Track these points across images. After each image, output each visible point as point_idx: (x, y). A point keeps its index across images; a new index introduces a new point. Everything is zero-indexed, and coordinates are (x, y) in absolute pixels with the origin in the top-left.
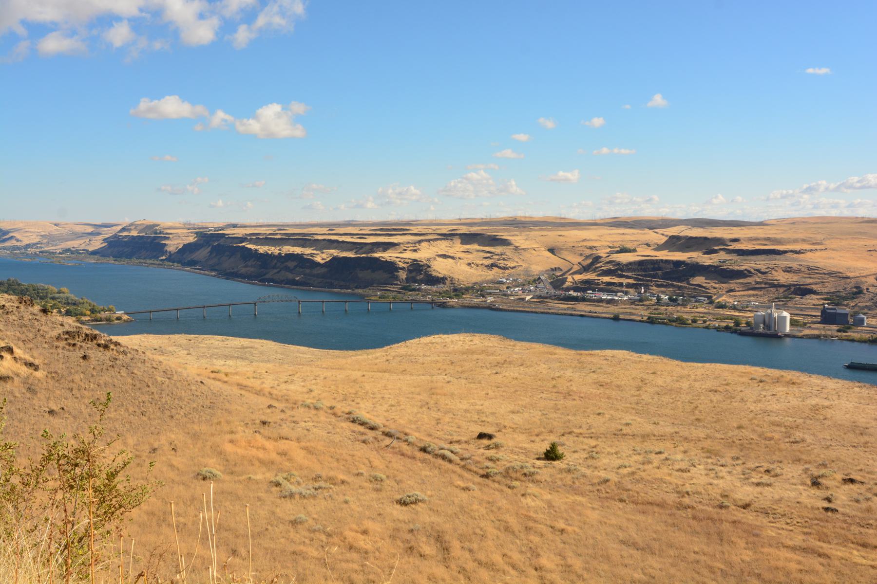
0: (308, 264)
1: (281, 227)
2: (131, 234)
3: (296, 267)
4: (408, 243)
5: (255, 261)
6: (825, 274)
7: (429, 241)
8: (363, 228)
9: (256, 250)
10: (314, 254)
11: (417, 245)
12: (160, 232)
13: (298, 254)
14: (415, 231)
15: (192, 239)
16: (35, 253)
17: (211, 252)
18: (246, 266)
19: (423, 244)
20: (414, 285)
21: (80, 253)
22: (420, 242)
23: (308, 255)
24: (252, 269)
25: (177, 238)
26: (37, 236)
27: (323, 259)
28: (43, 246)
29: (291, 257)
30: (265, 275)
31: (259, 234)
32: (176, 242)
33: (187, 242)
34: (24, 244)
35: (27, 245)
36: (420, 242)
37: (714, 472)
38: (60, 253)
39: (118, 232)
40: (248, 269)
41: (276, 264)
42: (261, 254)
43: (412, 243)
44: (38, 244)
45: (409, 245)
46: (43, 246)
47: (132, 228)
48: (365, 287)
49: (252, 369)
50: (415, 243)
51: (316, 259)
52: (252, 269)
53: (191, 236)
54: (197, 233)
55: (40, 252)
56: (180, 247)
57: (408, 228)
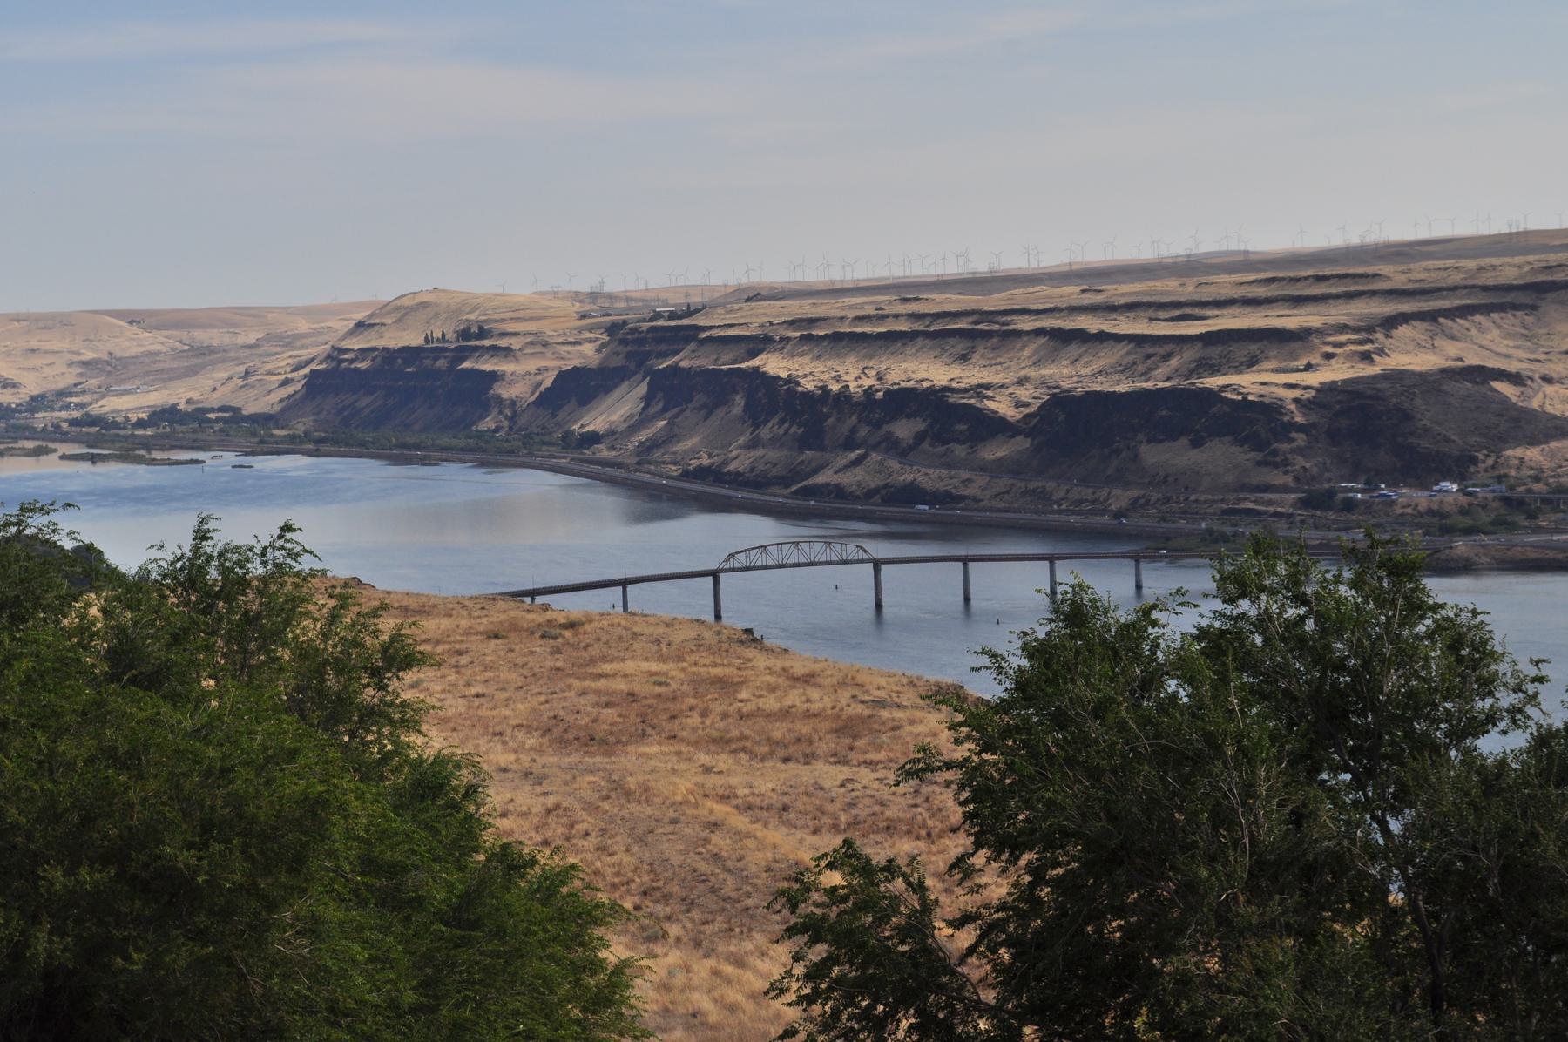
0: (962, 427)
1: (906, 290)
2: (380, 344)
3: (920, 437)
4: (1343, 328)
5: (782, 421)
6: (1277, 385)
7: (1431, 317)
8: (1203, 279)
9: (790, 380)
10: (988, 387)
11: (1379, 336)
12: (481, 328)
13: (931, 391)
14: (1399, 281)
15: (587, 354)
16: (57, 427)
17: (648, 399)
18: (753, 444)
19: (1404, 331)
20: (1346, 490)
21: (209, 421)
22: (1390, 323)
23: (965, 391)
24: (773, 454)
25: (539, 349)
26: (71, 364)
27: (1019, 404)
28: (86, 399)
29: (904, 400)
30: (815, 472)
31: (812, 322)
32: (532, 365)
33: (567, 365)
34: (22, 396)
35: (33, 398)
36: (1390, 323)
37: (270, 550)
38: (140, 424)
39: (343, 338)
40: (760, 452)
41: (853, 430)
42: (807, 395)
43: (1356, 330)
44: (70, 394)
45: (1343, 338)
46: (86, 399)
47: (388, 321)
48: (807, 479)
49: (799, 853)
50: (1370, 329)
51: (990, 404)
52: (773, 454)
53: (590, 341)
54: (612, 329)
55: (74, 423)
56: (548, 383)
57: (1370, 270)
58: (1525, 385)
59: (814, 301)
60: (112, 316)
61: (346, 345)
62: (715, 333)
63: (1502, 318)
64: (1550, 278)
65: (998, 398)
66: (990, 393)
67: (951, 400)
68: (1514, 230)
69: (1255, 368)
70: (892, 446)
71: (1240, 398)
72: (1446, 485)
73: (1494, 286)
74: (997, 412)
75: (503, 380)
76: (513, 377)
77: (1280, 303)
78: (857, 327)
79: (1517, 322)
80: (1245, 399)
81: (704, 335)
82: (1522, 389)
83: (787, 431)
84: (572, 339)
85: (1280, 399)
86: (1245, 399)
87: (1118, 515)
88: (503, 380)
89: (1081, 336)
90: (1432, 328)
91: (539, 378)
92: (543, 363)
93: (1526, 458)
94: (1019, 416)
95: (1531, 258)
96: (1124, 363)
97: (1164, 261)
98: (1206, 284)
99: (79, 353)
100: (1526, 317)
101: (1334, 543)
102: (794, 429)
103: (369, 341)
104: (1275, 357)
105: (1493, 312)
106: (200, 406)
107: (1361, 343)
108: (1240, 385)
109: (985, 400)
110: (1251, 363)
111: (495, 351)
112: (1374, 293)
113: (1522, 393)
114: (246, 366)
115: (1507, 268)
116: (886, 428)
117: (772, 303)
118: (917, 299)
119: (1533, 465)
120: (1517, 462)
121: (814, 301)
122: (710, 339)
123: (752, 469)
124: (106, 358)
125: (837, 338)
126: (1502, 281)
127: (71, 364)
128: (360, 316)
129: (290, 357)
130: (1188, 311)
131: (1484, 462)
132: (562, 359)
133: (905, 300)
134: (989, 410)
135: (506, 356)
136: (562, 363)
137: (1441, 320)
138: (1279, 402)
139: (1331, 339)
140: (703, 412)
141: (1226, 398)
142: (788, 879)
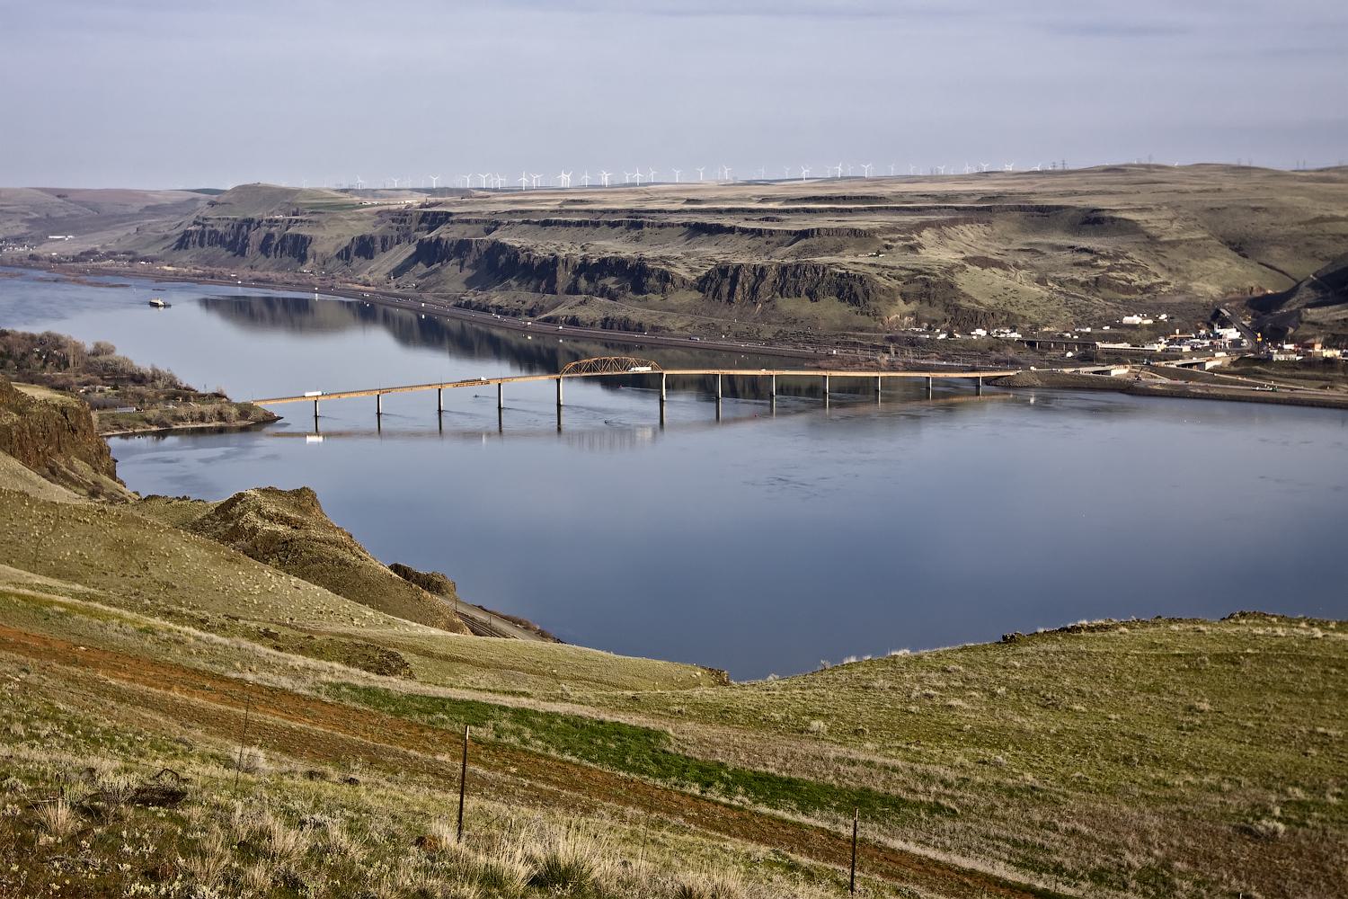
45: (897, 236)
64: (716, 222)
65: (678, 265)
68: (935, 174)
70: (604, 293)
79: (980, 230)
82: (1006, 272)
87: (769, 342)
89: (719, 229)
91: (339, 241)
94: (694, 278)
96: (752, 247)
99: (27, 214)
106: (111, 250)
110: (838, 250)
119: (1032, 321)
124: (45, 217)
125: (546, 223)
127: (22, 221)
137: (943, 227)
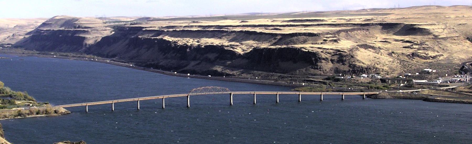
0: (229, 56)
3: (217, 58)
27: (243, 50)
36: (339, 32)
45: (329, 36)
54: (114, 27)
57: (322, 18)
58: (376, 50)
59: (169, 21)
60: (388, 13)
61: (42, 29)
62: (148, 29)
63: (361, 32)
66: (235, 47)
67: (225, 49)
69: (306, 43)
71: (307, 51)
72: (364, 75)
73: (357, 24)
74: (238, 52)
75: (87, 39)
76: (89, 38)
77: (301, 26)
78: (184, 28)
80: (308, 51)
81: (144, 29)
82: (376, 51)
83: (176, 55)
84: (104, 29)
85: (318, 51)
86: (308, 51)
88: (87, 39)
90: (347, 34)
92: (97, 35)
93: (384, 69)
95: (362, 17)
97: (270, 14)
98: (275, 21)
100: (366, 32)
101: (342, 90)
102: (178, 55)
103: (281, 32)
104: (311, 40)
105: (358, 30)
107: (333, 37)
108: (306, 48)
109: (234, 49)
110: (304, 42)
111: (84, 32)
112: (325, 24)
113: (376, 52)
114: (13, 33)
115: (357, 19)
116: (205, 56)
117: (158, 21)
118: (197, 22)
120: (382, 70)
121: (169, 21)
122: (146, 30)
123: (167, 65)
126: (356, 23)
128: (43, 21)
129: (25, 31)
130: (278, 27)
131: (373, 70)
132: (102, 34)
133: (194, 22)
134: (236, 52)
135: (87, 33)
136: (102, 35)
137: (348, 32)
138: (317, 52)
139: (326, 36)
140: (146, 49)
141: (303, 51)
142: (3, 116)
